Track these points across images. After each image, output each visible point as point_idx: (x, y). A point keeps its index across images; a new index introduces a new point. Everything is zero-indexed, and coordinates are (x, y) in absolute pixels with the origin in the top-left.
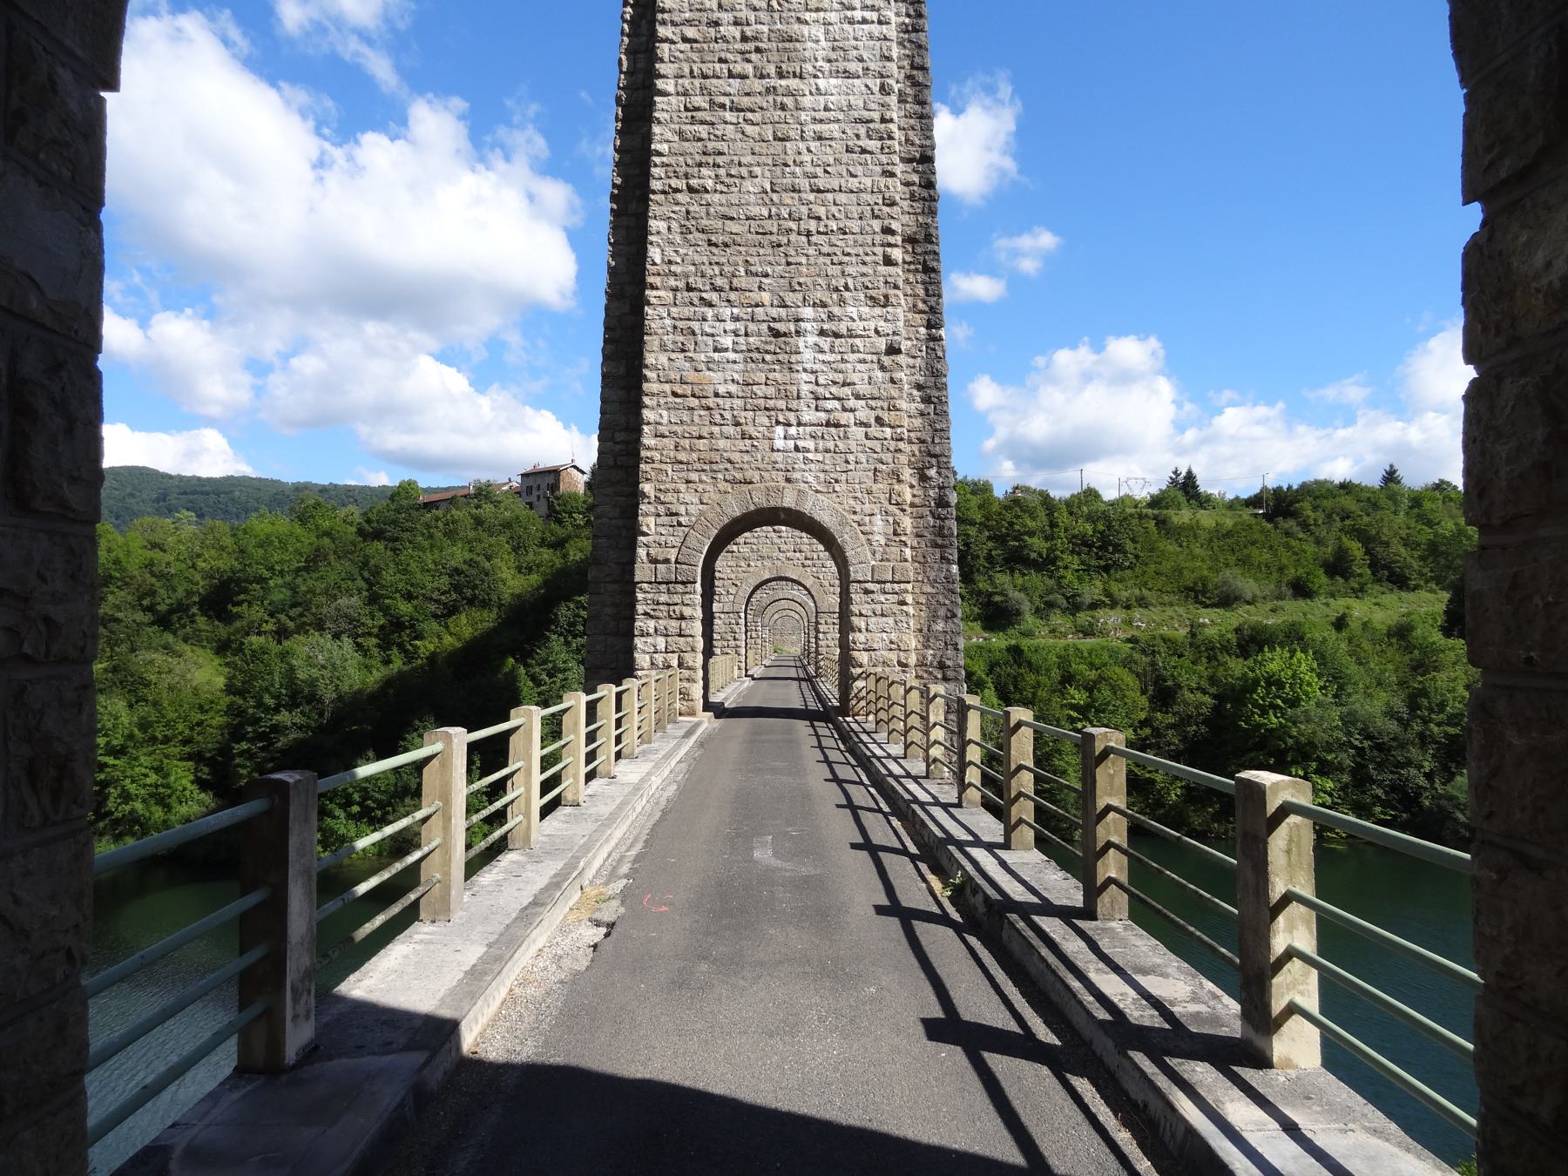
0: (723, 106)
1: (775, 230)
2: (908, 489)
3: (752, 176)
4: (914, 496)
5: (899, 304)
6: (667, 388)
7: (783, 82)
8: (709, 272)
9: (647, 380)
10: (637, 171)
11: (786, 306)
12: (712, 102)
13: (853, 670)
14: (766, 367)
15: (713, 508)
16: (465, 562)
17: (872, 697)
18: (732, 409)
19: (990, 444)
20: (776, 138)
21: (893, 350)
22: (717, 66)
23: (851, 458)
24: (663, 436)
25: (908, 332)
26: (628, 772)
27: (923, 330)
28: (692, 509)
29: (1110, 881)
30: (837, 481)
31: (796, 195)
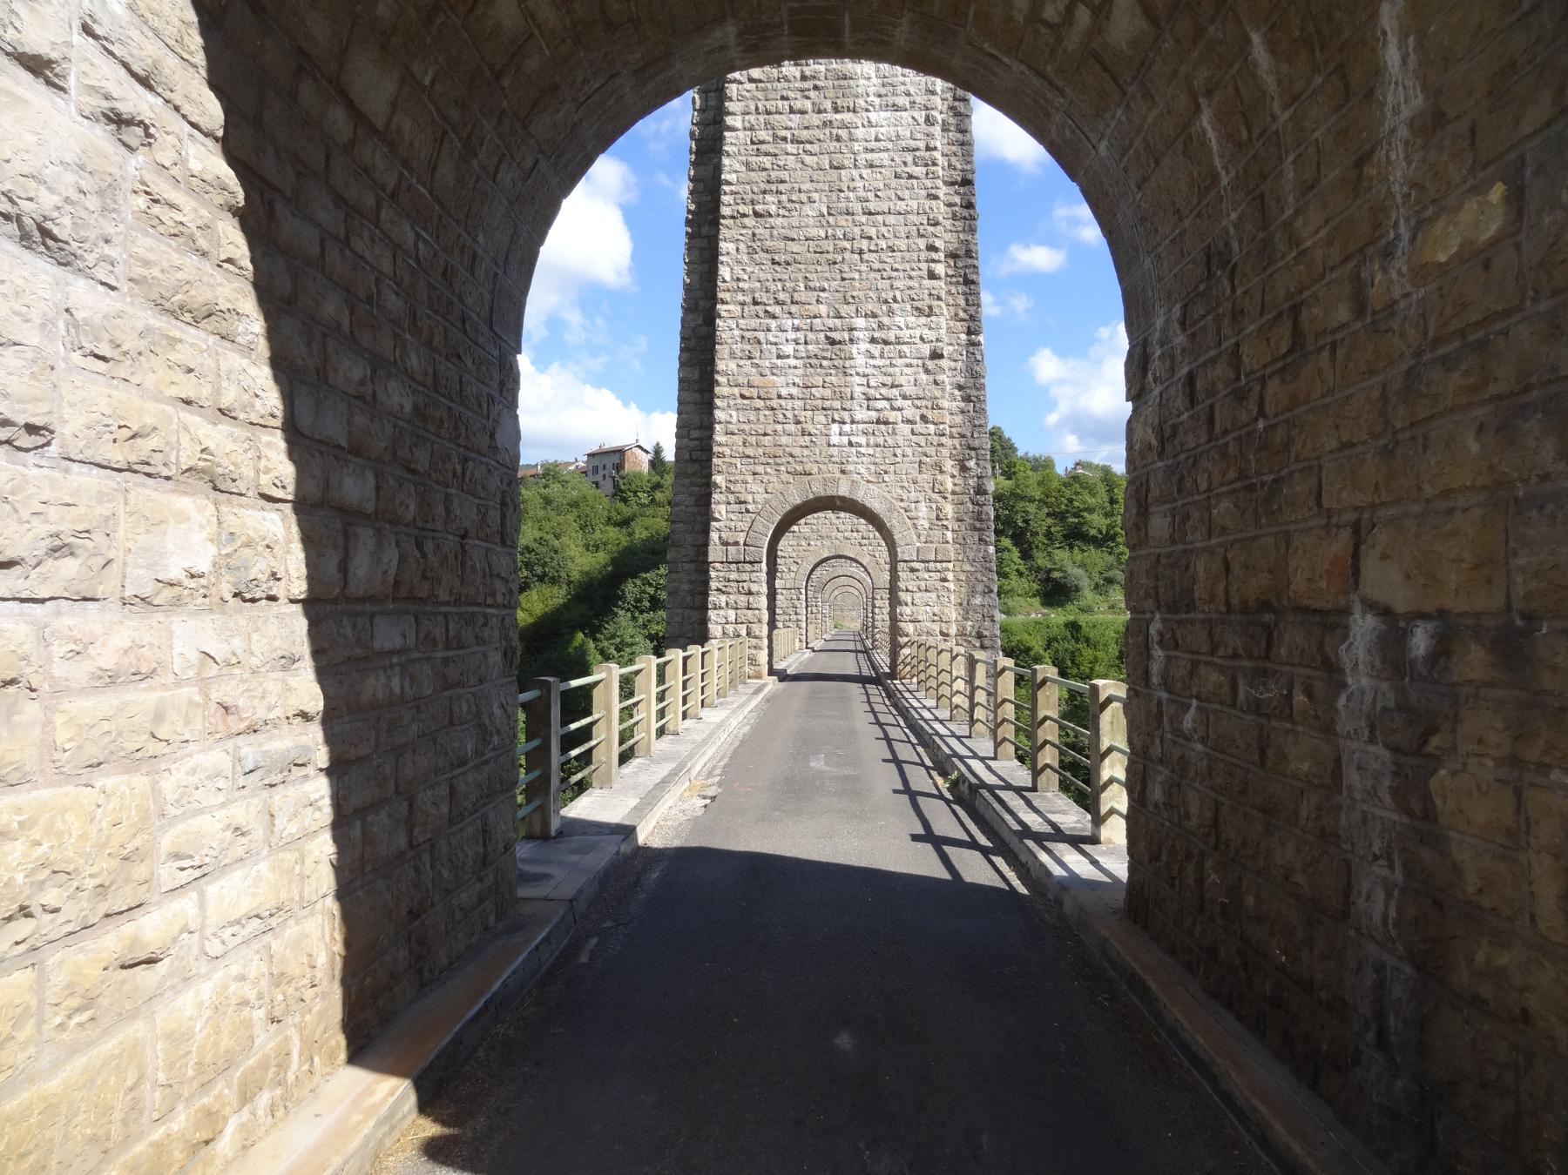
0: (784, 139)
1: (831, 249)
2: (950, 479)
3: (811, 201)
4: (955, 485)
5: (942, 314)
6: (736, 391)
7: (839, 116)
8: (773, 288)
9: (719, 385)
10: (709, 198)
11: (841, 317)
12: (775, 136)
13: (900, 639)
14: (823, 371)
15: (776, 496)
16: (535, 540)
17: (915, 662)
18: (793, 409)
19: (1053, 418)
20: (832, 167)
21: (936, 355)
22: (780, 103)
23: (899, 452)
24: (733, 434)
25: (950, 338)
26: (711, 716)
27: (964, 337)
28: (759, 498)
29: (1047, 766)
30: (886, 472)
31: (850, 218)
